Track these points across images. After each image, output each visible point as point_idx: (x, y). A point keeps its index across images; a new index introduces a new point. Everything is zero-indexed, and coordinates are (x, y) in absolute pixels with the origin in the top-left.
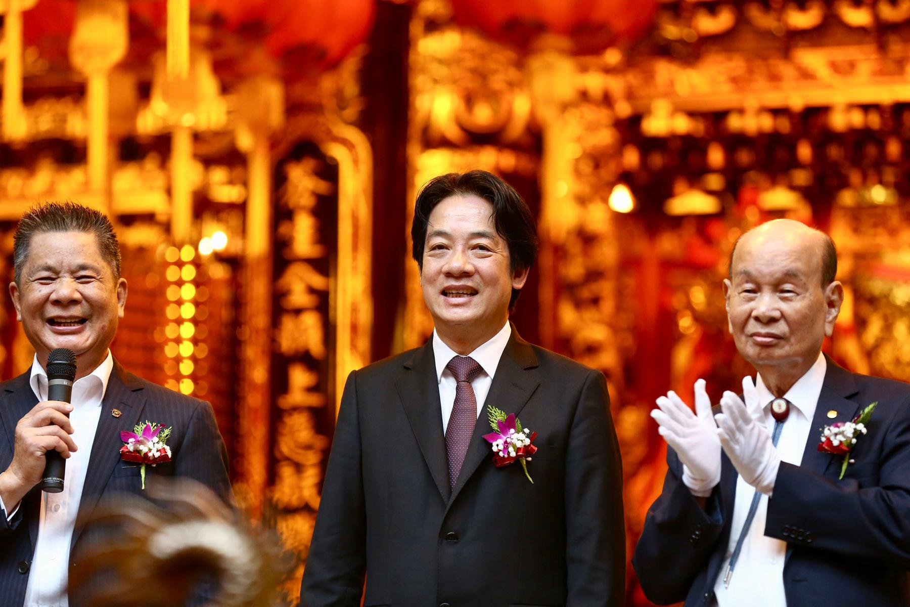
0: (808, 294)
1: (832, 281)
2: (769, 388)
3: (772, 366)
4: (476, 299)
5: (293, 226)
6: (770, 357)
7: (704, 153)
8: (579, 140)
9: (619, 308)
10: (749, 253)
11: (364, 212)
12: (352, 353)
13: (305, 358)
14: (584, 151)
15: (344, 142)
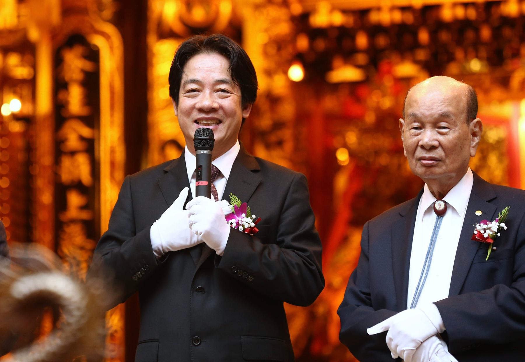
0: (457, 128)
1: (475, 118)
2: (433, 193)
3: (435, 179)
4: (221, 126)
5: (68, 94)
6: (432, 173)
7: (353, 38)
8: (266, 30)
9: (296, 149)
10: (416, 101)
11: (119, 85)
12: (111, 182)
13: (78, 186)
14: (270, 38)
15: (103, 34)
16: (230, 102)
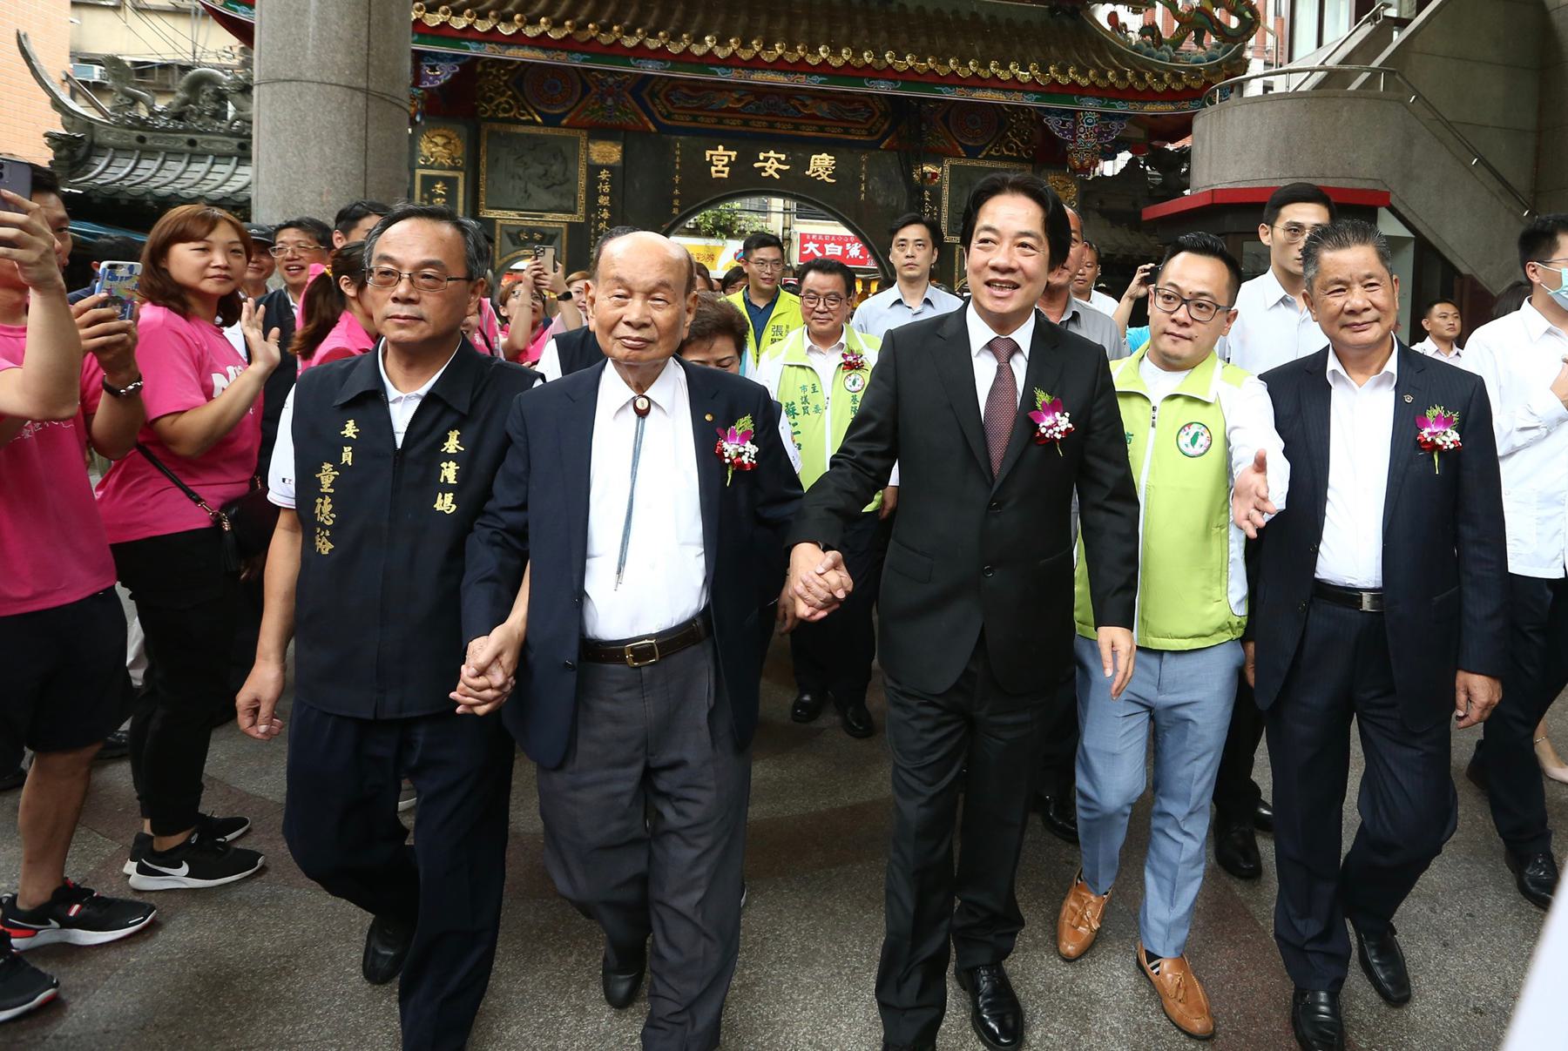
4: (1018, 292)
16: (1032, 262)
